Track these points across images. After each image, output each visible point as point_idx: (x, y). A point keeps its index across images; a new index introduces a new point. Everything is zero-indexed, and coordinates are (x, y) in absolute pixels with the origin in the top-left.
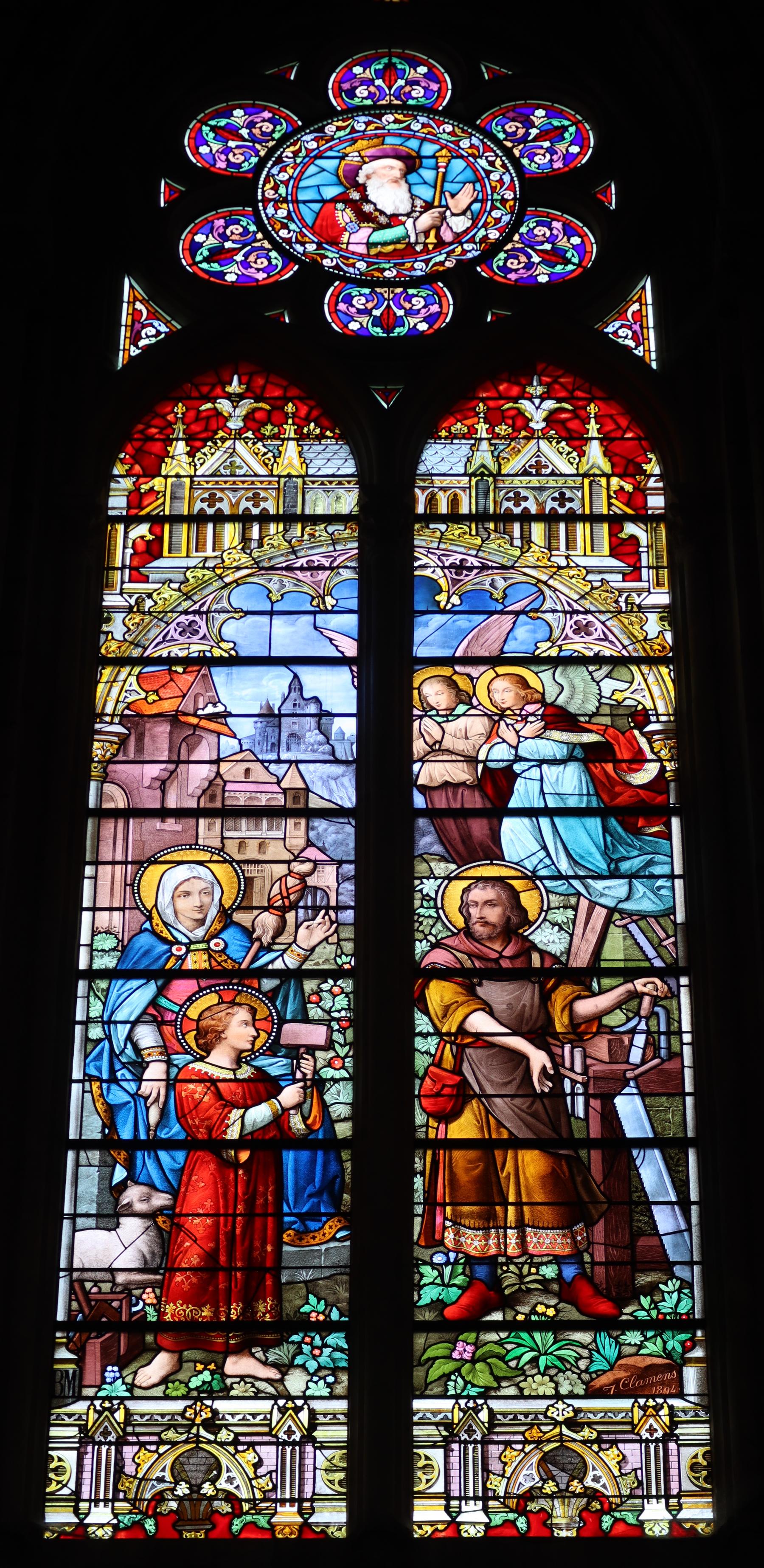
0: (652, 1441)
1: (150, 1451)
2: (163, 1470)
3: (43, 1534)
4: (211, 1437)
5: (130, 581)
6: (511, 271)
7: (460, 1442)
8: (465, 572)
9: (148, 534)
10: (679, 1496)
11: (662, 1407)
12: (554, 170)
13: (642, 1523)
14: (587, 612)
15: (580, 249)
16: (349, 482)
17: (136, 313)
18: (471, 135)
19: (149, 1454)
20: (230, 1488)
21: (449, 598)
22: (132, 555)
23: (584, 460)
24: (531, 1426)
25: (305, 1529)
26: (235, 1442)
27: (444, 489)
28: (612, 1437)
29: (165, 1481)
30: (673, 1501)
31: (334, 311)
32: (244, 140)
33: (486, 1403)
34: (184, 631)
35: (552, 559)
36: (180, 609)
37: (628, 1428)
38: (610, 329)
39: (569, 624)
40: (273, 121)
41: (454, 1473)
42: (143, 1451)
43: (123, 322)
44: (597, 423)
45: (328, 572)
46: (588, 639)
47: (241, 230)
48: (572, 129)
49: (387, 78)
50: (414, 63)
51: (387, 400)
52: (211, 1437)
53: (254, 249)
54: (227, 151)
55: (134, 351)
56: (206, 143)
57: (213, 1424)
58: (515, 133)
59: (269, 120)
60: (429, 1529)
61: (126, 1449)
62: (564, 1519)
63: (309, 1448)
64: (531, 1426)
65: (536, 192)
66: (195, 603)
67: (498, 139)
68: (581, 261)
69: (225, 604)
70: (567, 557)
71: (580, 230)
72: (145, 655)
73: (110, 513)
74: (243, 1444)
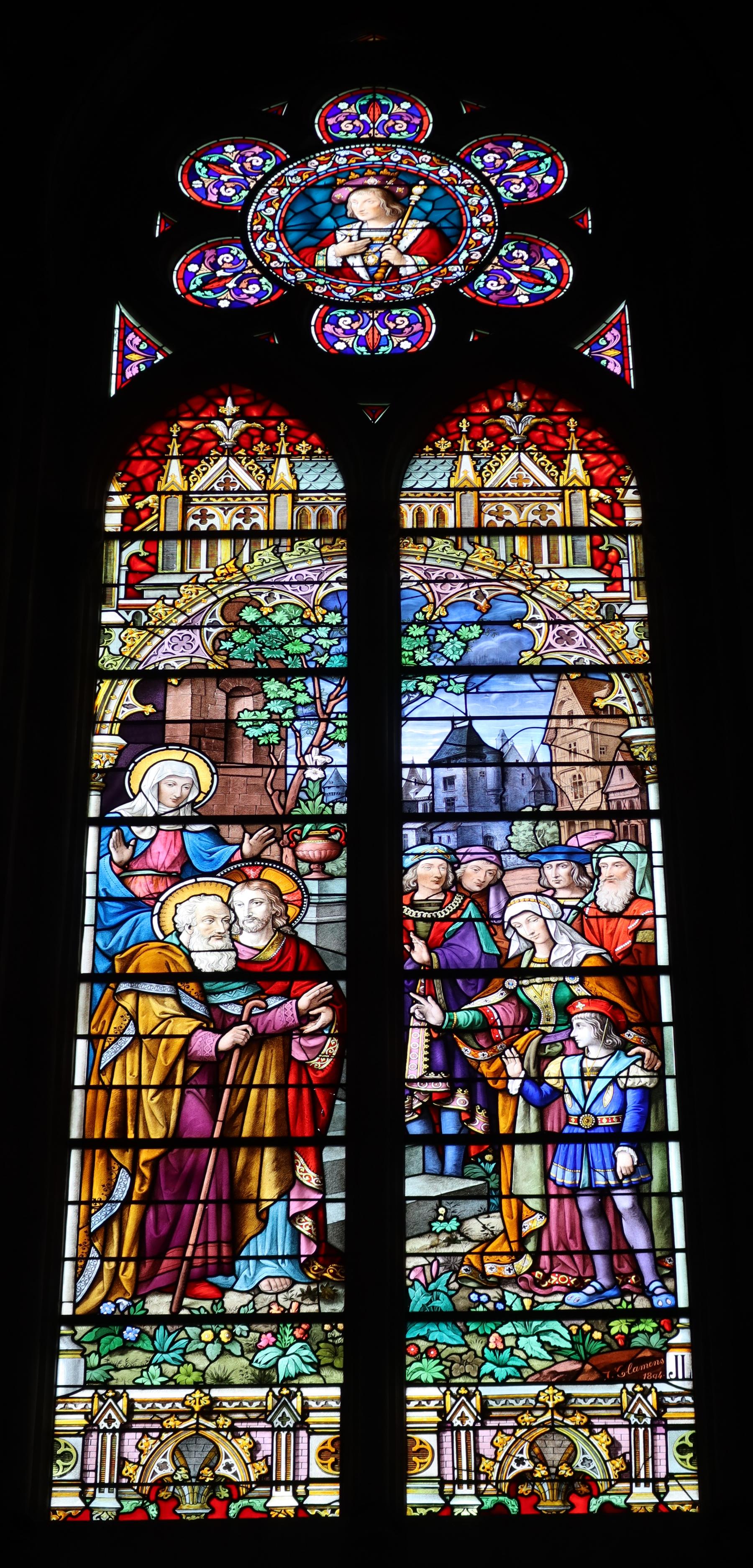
0: (463, 1428)
2: (165, 1456)
3: (49, 1517)
5: (126, 598)
6: (259, 155)
9: (141, 551)
10: (666, 1480)
14: (568, 622)
15: (557, 271)
19: (507, 1438)
20: (228, 1474)
21: (435, 609)
23: (565, 473)
31: (322, 334)
35: (536, 572)
39: (552, 633)
45: (317, 586)
46: (570, 648)
47: (512, 188)
48: (548, 160)
51: (373, 419)
53: (245, 276)
54: (219, 184)
56: (198, 178)
60: (61, 1514)
61: (128, 1436)
63: (303, 1434)
65: (515, 220)
68: (559, 282)
70: (549, 569)
72: (141, 668)
74: (598, 1426)
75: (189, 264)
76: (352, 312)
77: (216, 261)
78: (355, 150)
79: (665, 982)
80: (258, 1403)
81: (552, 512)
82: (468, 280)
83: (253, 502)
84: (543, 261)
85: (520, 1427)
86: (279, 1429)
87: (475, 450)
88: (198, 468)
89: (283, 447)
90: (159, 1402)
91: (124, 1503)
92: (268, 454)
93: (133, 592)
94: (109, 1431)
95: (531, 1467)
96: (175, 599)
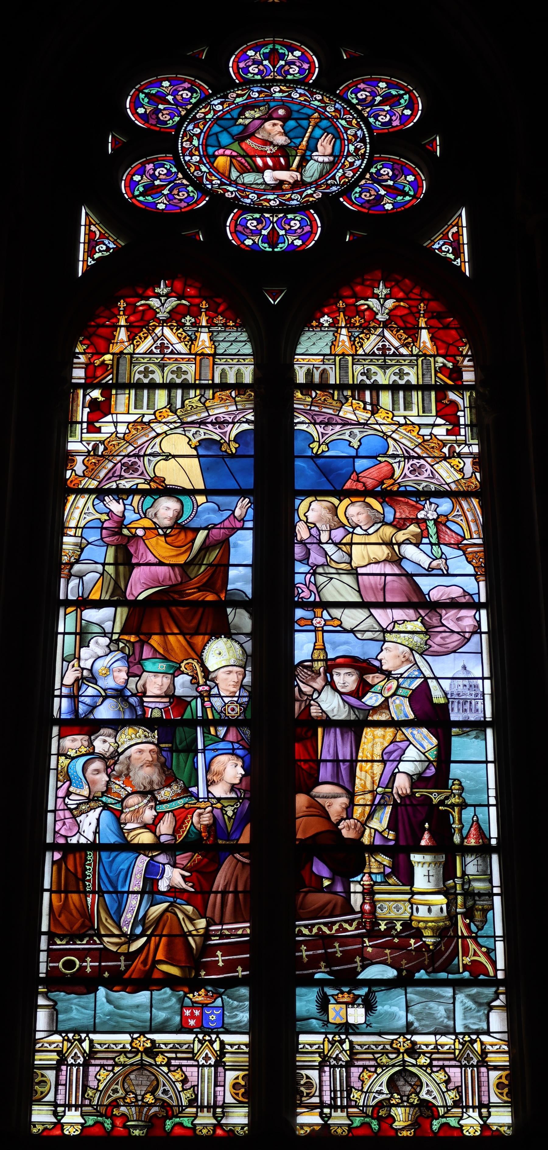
4: (414, 1062)
5: (88, 432)
7: (331, 1066)
8: (331, 427)
9: (100, 396)
12: (393, 127)
13: (462, 1126)
14: (419, 457)
17: (90, 234)
18: (336, 102)
20: (165, 1097)
28: (441, 1063)
29: (383, 1093)
32: (170, 103)
34: (415, 470)
35: (395, 419)
36: (123, 454)
37: (190, 1055)
38: (436, 246)
40: (192, 91)
42: (102, 1071)
45: (231, 426)
48: (406, 97)
49: (272, 60)
50: (292, 49)
51: (271, 297)
52: (414, 1062)
55: (91, 262)
57: (413, 1051)
58: (364, 100)
59: (189, 89)
61: (353, 1070)
65: (384, 143)
68: (415, 193)
69: (157, 449)
70: (405, 417)
73: (73, 381)
77: (154, 173)
78: (265, 87)
84: (403, 177)
87: (350, 326)
88: (141, 334)
92: (193, 325)
93: (93, 429)
94: (75, 1065)
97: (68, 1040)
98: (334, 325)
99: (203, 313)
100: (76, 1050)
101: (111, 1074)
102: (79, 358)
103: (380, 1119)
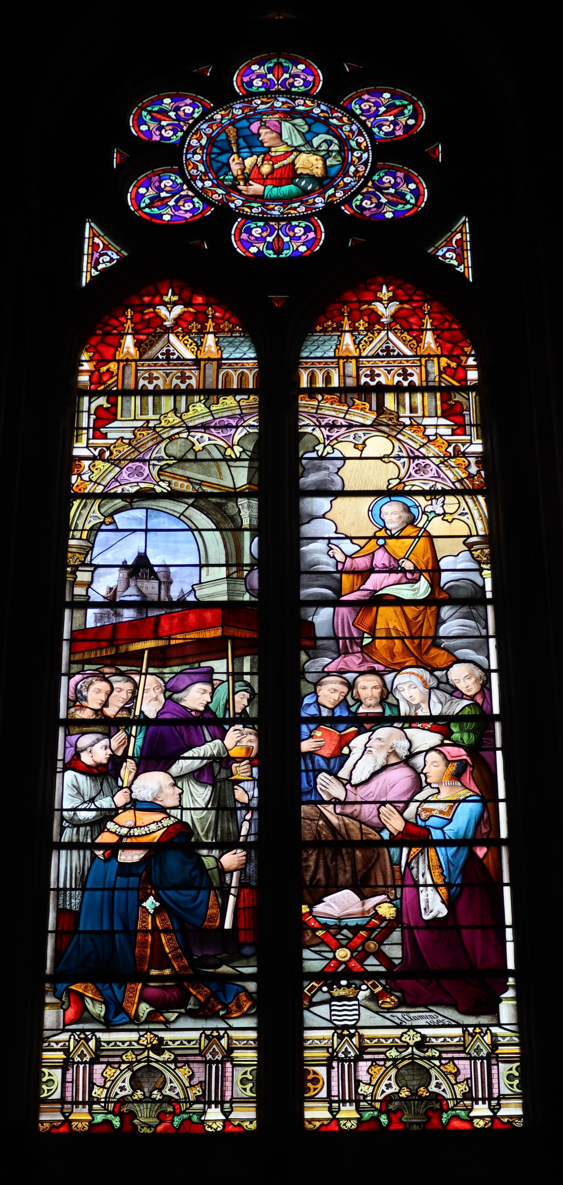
0: (479, 1058)
1: (379, 1065)
2: (390, 1079)
4: (422, 1054)
5: (94, 438)
6: (190, 105)
8: (336, 430)
11: (223, 1037)
12: (396, 136)
14: (425, 457)
16: (332, 363)
17: (95, 246)
19: (114, 1070)
22: (94, 420)
24: (127, 1050)
25: (227, 1123)
26: (175, 1061)
27: (321, 369)
28: (185, 1059)
30: (494, 1103)
33: (356, 1031)
34: (419, 470)
35: (401, 419)
37: (461, 1049)
38: (440, 253)
41: (334, 1084)
42: (109, 1068)
43: (86, 252)
44: (349, 320)
45: (234, 430)
47: (171, 183)
48: (410, 107)
51: (280, 308)
52: (422, 1054)
54: (160, 128)
55: (95, 273)
56: (412, 191)
57: (159, 1047)
58: (368, 110)
60: (47, 1125)
61: (96, 1067)
62: (145, 1117)
64: (127, 1050)
66: (141, 453)
67: (356, 114)
70: (410, 418)
71: (415, 178)
74: (445, 1059)
75: (139, 188)
76: (293, 89)
78: (290, 99)
79: (498, 726)
80: (457, 1039)
81: (411, 375)
82: (347, 201)
83: (409, 364)
85: (124, 1062)
86: (475, 1059)
87: (354, 330)
89: (210, 325)
90: (434, 1037)
91: (363, 1114)
93: (99, 434)
94: (479, 1058)
95: (397, 1091)
96: (130, 439)
97: (470, 1034)
98: (339, 329)
99: (346, 319)
100: (346, 1046)
101: (118, 1071)
102: (82, 365)
103: (121, 1115)
